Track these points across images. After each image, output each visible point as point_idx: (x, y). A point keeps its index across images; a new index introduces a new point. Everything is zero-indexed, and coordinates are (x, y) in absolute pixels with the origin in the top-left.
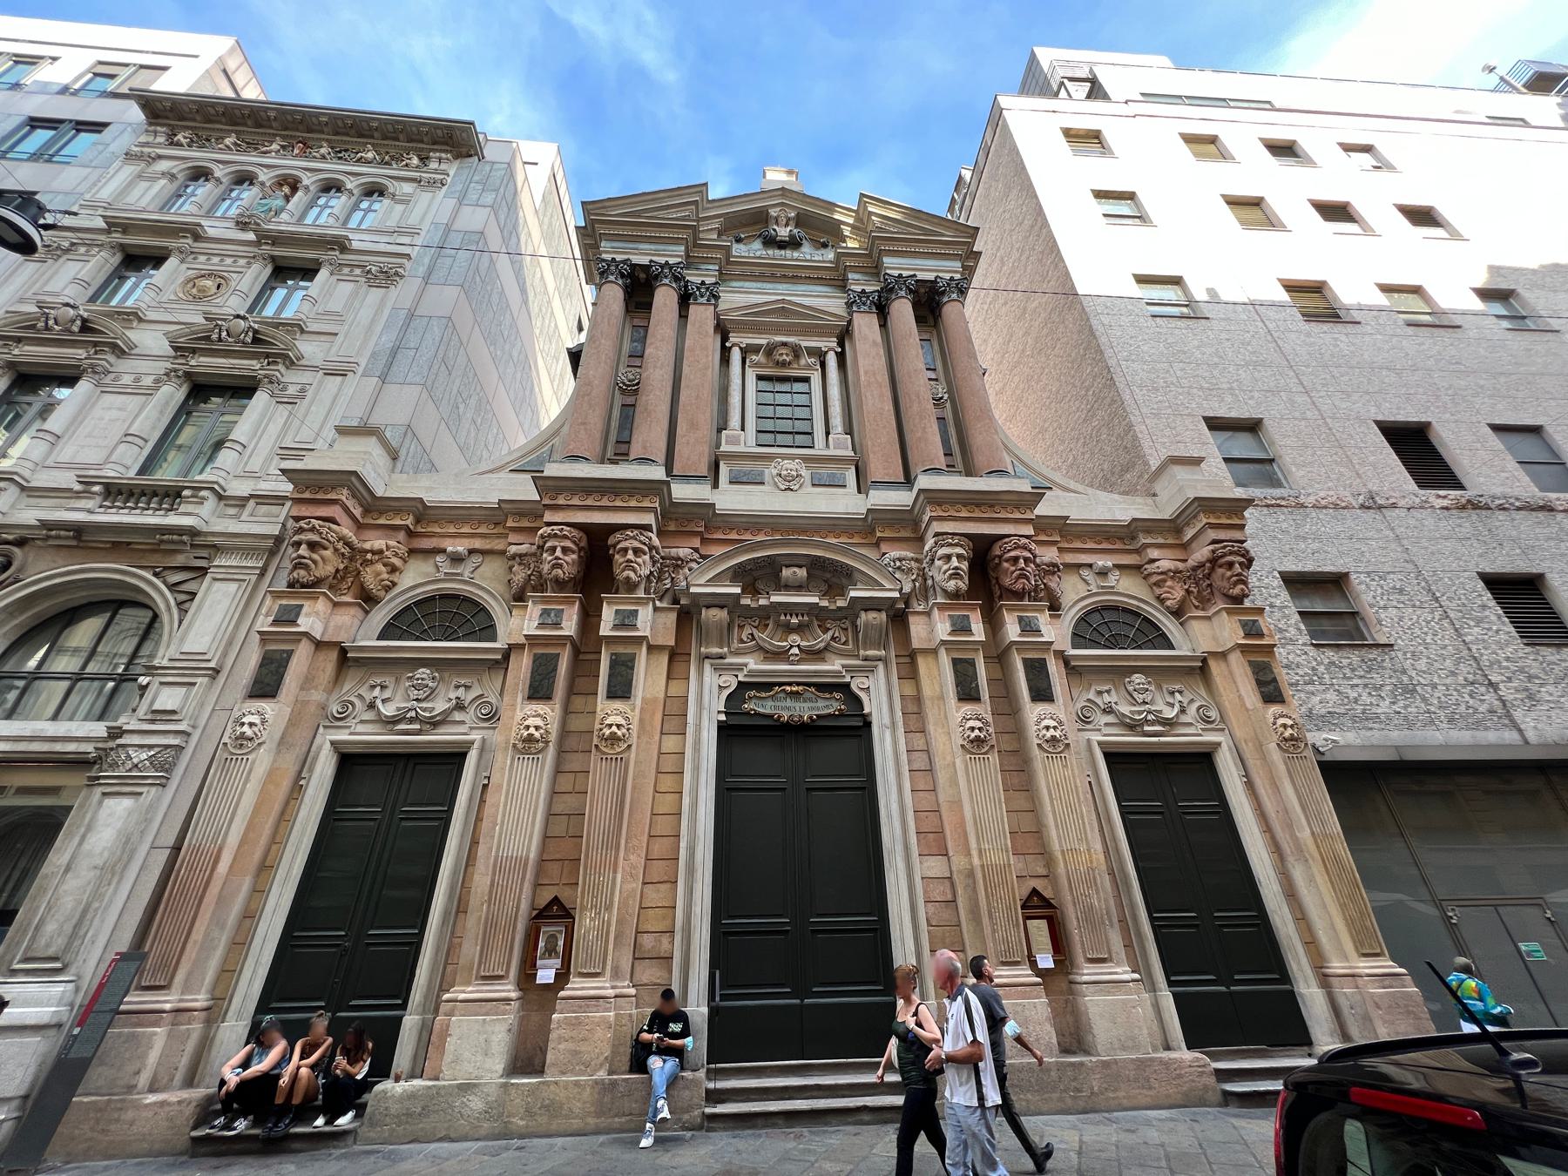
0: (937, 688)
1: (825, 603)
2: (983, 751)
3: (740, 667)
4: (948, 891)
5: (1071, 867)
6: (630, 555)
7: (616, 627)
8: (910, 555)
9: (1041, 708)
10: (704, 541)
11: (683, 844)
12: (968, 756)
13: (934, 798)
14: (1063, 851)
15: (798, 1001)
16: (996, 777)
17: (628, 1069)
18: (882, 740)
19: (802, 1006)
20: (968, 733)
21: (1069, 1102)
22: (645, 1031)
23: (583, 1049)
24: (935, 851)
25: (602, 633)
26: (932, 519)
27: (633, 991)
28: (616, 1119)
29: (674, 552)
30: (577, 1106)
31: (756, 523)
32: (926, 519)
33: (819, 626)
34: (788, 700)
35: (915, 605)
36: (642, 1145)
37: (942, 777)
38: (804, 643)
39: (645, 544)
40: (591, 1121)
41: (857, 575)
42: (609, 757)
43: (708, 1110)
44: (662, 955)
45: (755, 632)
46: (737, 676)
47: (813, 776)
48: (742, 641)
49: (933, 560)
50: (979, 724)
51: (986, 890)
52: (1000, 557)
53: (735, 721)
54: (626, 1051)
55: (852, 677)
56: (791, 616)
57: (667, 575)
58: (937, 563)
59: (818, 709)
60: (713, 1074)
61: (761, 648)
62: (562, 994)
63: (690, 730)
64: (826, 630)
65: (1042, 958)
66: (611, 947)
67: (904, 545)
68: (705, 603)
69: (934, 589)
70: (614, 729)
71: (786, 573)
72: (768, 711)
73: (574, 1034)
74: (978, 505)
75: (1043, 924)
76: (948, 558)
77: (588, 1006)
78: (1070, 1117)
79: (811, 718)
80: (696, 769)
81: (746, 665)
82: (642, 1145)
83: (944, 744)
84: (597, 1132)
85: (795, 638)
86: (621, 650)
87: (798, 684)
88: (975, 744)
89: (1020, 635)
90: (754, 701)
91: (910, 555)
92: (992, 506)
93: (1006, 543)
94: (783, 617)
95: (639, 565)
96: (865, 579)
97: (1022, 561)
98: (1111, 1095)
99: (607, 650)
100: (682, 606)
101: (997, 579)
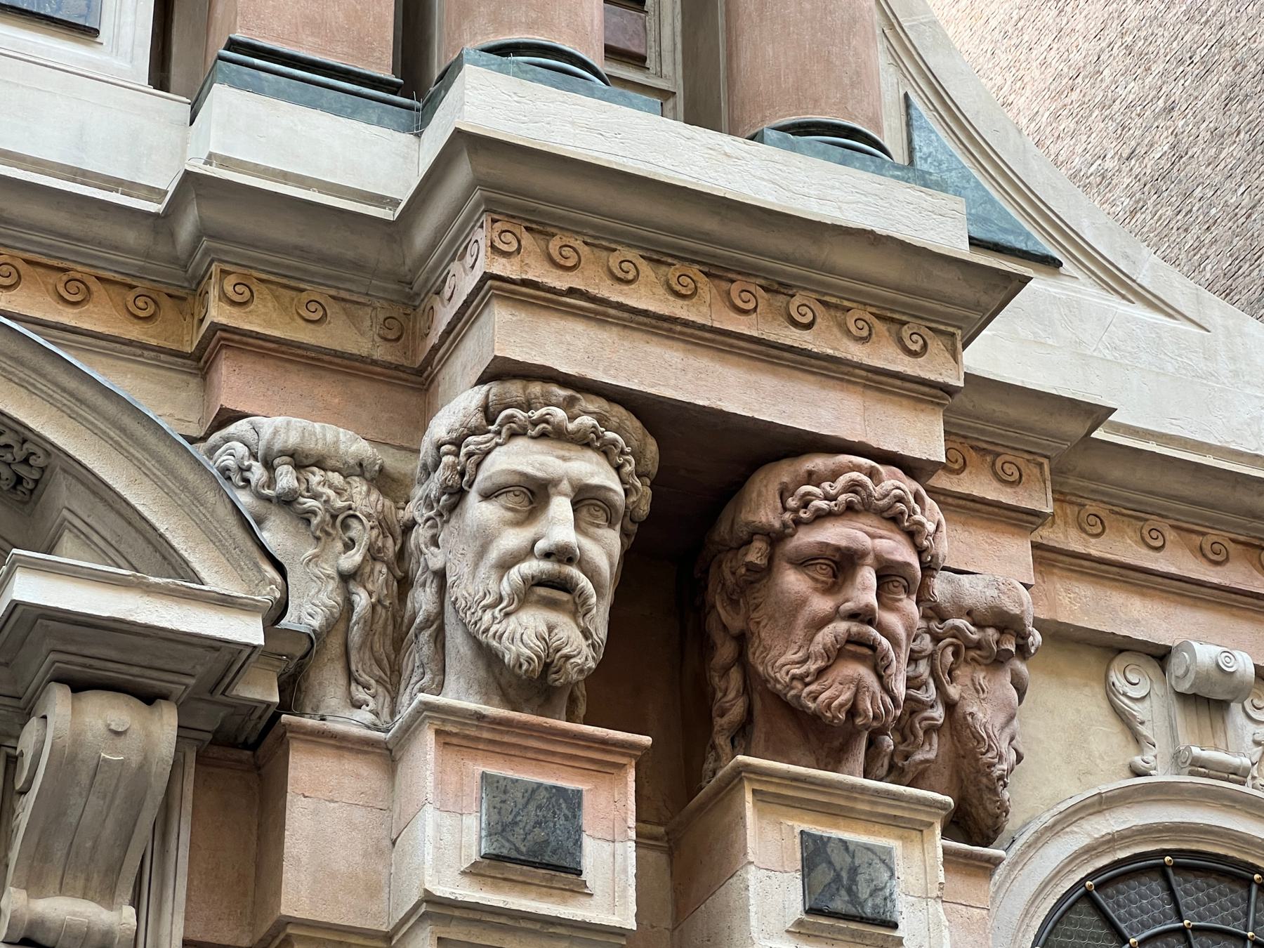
32: (463, 281)
49: (456, 495)
52: (775, 538)
58: (478, 511)
67: (327, 390)
74: (717, 271)
91: (354, 445)
93: (811, 478)
96: (107, 524)
101: (742, 640)
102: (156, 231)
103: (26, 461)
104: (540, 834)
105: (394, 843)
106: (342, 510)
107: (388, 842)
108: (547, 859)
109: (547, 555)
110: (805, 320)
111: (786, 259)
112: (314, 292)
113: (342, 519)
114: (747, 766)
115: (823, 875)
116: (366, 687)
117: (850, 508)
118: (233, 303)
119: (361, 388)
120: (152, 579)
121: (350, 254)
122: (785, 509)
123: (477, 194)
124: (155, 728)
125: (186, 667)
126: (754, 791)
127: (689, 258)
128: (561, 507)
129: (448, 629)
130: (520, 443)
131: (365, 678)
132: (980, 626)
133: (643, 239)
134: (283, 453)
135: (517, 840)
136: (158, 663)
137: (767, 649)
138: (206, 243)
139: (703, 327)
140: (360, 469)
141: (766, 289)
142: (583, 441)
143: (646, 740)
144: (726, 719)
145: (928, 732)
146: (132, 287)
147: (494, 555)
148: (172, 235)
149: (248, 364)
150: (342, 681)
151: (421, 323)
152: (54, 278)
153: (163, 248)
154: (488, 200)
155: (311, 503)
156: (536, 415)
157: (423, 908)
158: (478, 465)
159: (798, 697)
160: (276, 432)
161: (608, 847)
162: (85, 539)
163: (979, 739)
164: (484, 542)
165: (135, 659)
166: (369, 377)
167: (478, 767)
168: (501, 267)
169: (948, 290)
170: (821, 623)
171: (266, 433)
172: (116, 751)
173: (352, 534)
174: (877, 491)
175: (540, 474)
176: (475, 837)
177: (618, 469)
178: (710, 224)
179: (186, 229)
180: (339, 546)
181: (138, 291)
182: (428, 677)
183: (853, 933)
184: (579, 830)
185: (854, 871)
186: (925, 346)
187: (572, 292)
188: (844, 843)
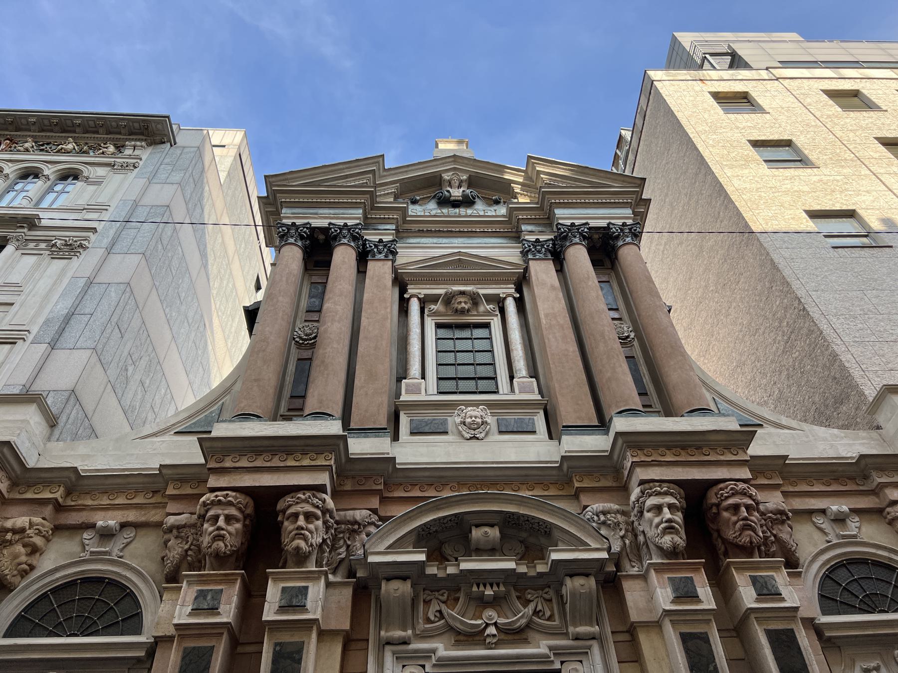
1: (523, 569)
8: (616, 507)
10: (384, 500)
26: (634, 465)
31: (442, 477)
33: (518, 598)
35: (628, 566)
38: (502, 621)
39: (317, 507)
41: (556, 534)
45: (444, 608)
46: (423, 666)
48: (428, 621)
52: (718, 505)
55: (562, 663)
56: (485, 586)
57: (342, 542)
58: (648, 515)
61: (450, 629)
64: (526, 603)
71: (477, 534)
74: (684, 448)
76: (658, 509)
81: (434, 651)
85: (491, 614)
92: (699, 448)
93: (721, 489)
94: (475, 589)
95: (311, 532)
97: (743, 509)
99: (270, 640)
101: (718, 531)
103: (546, 527)
104: (686, 589)
109: (666, 522)
112: (595, 475)
116: (634, 562)
126: (734, 568)
127: (676, 447)
131: (634, 560)
134: (600, 512)
138: (570, 470)
139: (684, 461)
140: (618, 512)
141: (696, 449)
142: (666, 494)
147: (654, 524)
148: (562, 470)
154: (626, 446)
155: (609, 522)
156: (653, 490)
157: (664, 613)
158: (644, 505)
164: (651, 522)
168: (635, 459)
171: (595, 509)
176: (671, 593)
177: (676, 498)
178: (679, 438)
180: (618, 530)
184: (695, 587)
185: (766, 583)
187: (652, 461)
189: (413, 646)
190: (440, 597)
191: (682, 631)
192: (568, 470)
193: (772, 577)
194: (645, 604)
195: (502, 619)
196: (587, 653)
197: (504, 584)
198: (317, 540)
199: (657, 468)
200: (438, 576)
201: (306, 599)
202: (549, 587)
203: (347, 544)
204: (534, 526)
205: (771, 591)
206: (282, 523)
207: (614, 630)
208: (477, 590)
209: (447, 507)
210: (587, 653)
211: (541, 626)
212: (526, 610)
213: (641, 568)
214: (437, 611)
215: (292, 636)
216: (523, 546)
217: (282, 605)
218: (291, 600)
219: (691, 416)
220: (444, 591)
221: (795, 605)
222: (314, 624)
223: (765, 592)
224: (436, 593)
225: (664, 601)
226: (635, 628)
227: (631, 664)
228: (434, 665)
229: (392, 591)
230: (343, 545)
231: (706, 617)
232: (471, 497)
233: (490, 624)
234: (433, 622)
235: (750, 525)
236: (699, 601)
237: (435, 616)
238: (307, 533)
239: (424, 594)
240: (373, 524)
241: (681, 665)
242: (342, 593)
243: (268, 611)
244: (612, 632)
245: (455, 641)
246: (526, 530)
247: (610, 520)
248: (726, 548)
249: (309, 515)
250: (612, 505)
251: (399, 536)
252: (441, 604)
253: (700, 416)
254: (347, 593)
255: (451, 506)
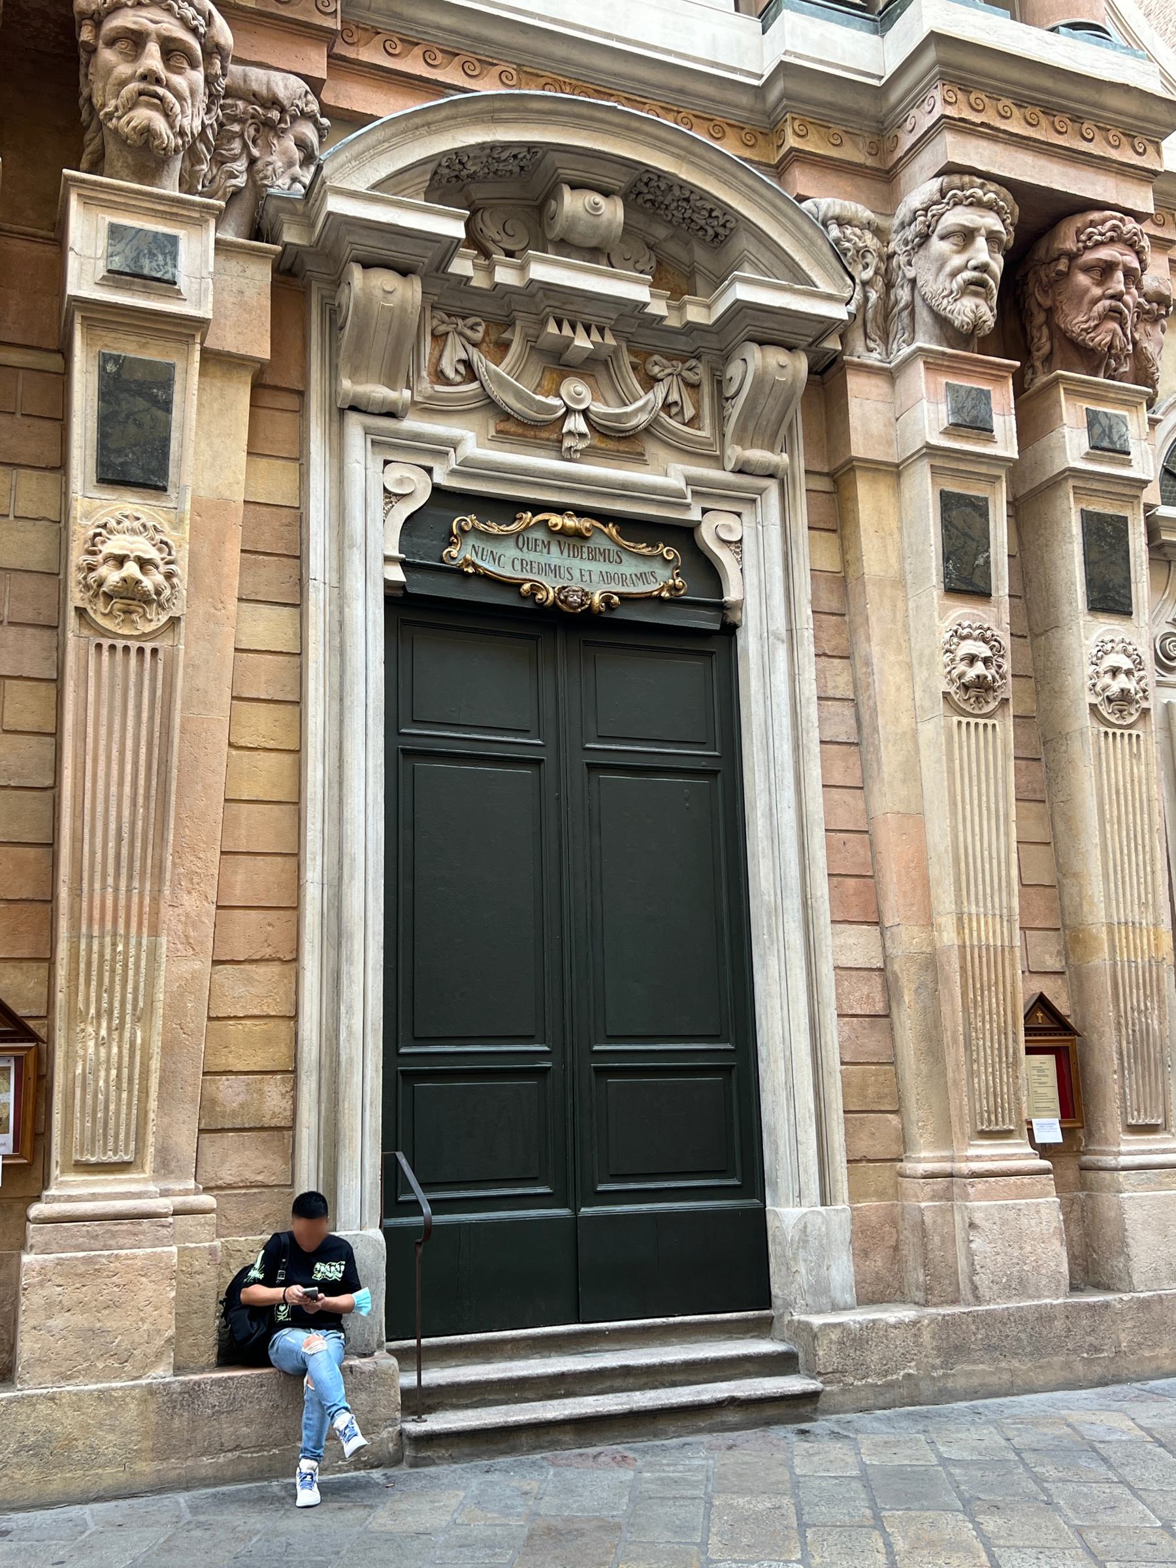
0: (893, 560)
1: (658, 308)
2: (987, 709)
3: (441, 448)
4: (878, 996)
5: (1122, 957)
6: (152, 59)
7: (115, 278)
8: (866, 214)
9: (1106, 627)
10: (336, 62)
11: (313, 874)
12: (956, 719)
13: (861, 805)
14: (1110, 926)
15: (564, 1212)
16: (1005, 768)
17: (213, 1359)
18: (767, 671)
19: (576, 1220)
20: (962, 667)
21: (1080, 1368)
22: (256, 1281)
23: (110, 1324)
24: (855, 915)
25: (72, 289)
26: (946, 123)
27: (208, 1200)
28: (205, 1460)
29: (258, 78)
30: (108, 1441)
31: (479, 40)
32: (923, 119)
33: (635, 368)
34: (554, 549)
35: (860, 347)
36: (300, 1503)
37: (889, 758)
38: (598, 408)
39: (194, 31)
40: (146, 1468)
41: (744, 243)
42: (120, 644)
43: (414, 1427)
44: (267, 1121)
45: (476, 356)
46: (429, 471)
47: (602, 738)
48: (440, 377)
49: (925, 237)
50: (983, 650)
51: (964, 994)
52: (1072, 257)
53: (427, 586)
54: (209, 1323)
55: (705, 511)
56: (573, 328)
57: (237, 145)
58: (937, 245)
59: (623, 579)
60: (416, 1359)
61: (490, 404)
62: (36, 1210)
63: (317, 598)
64: (650, 382)
65: (1042, 1125)
66: (153, 1104)
67: (845, 183)
68: (361, 252)
69: (912, 314)
70: (132, 569)
71: (573, 203)
72: (505, 571)
73: (86, 1294)
74: (1049, 110)
75: (1048, 1062)
76: (966, 236)
77: (114, 1235)
78: (1083, 1393)
79: (607, 600)
80: (339, 696)
81: (455, 444)
82: (300, 1503)
83: (898, 689)
84: (160, 1488)
85: (576, 390)
86: (129, 348)
87: (581, 512)
88: (972, 692)
89: (1088, 457)
90: (471, 541)
91: (866, 214)
92: (1077, 119)
93: (1092, 224)
94: (552, 328)
95: (179, 97)
96: (766, 258)
97: (1120, 275)
98: (1147, 1354)
99: (88, 343)
100: (286, 246)
101: (1050, 312)
102: (756, 96)
103: (724, 226)
104: (974, 412)
105: (897, 419)
106: (862, 248)
107: (893, 420)
108: (979, 425)
109: (975, 268)
110: (1090, 137)
111: (1082, 102)
112: (836, 129)
113: (862, 253)
114: (1062, 376)
115: (1097, 430)
116: (874, 341)
117: (1112, 240)
118: (799, 136)
119: (860, 181)
120: (797, 286)
121: (856, 106)
122: (1078, 241)
123: (937, 69)
124: (797, 363)
125: (808, 332)
126: (1065, 389)
127: (1035, 103)
128: (981, 242)
129: (917, 309)
130: (959, 209)
131: (873, 336)
132: (1149, 302)
133: (1015, 93)
134: (832, 218)
135: (964, 415)
136: (801, 332)
137: (1067, 316)
138: (785, 102)
139: (1043, 142)
140: (868, 226)
141: (1071, 120)
142: (990, 207)
143: (1018, 364)
144: (1041, 353)
145: (1125, 357)
146: (743, 129)
147: (948, 269)
148: (764, 99)
149: (808, 169)
150: (863, 338)
151: (888, 145)
152: (706, 124)
153: (759, 106)
154: (941, 73)
155: (847, 245)
156: (968, 193)
157: (924, 450)
158: (937, 221)
159: (1084, 340)
160: (829, 207)
161: (1001, 418)
162: (756, 267)
163: (1148, 360)
164: (942, 262)
165: (786, 328)
166: (864, 176)
167: (943, 380)
168: (950, 111)
169: (1159, 117)
170: (1096, 301)
171: (823, 207)
172: (782, 376)
173: (868, 260)
174: (1125, 229)
175: (971, 225)
176: (945, 415)
177: (1003, 221)
178: (1048, 83)
179: (774, 95)
180: (861, 267)
181: (746, 131)
182: (906, 335)
183: (1111, 458)
184: (991, 410)
185: (1111, 427)
186: (1145, 150)
187: (983, 124)
188: (1105, 413)
189: (411, 424)
190: (469, 332)
191: (947, 489)
192: (780, 100)
193: (1123, 420)
194: (882, 428)
195: (600, 405)
196: (754, 501)
197: (616, 333)
198: (193, 119)
199: (984, 144)
200: (473, 283)
201: (175, 266)
202: (698, 358)
203: (249, 154)
204: (695, 216)
205: (1115, 443)
206: (93, 51)
207: (811, 469)
208: (557, 332)
209: (515, 121)
210: (754, 501)
211: (674, 434)
212: (650, 395)
213: (884, 355)
214: (460, 361)
215: (144, 346)
216: (654, 258)
217: (115, 267)
218: (136, 259)
219: (1074, 37)
220: (479, 320)
221: (1144, 477)
222: (197, 329)
223: (1105, 443)
224: (460, 322)
225: (930, 426)
226: (853, 469)
227: (823, 534)
228: (453, 472)
229: (378, 293)
230: (241, 153)
231: (996, 472)
232: (577, 109)
233: (575, 411)
234: (448, 382)
235: (1121, 313)
236: (991, 440)
237: (457, 371)
238: (170, 97)
239: (433, 317)
240: (310, 117)
241: (933, 548)
242: (248, 273)
243: (80, 278)
244: (807, 472)
245: (498, 432)
246: (670, 222)
247: (849, 241)
248: (1051, 352)
249: (172, 46)
250: (860, 207)
251: (401, 165)
252: (470, 348)
253: (1088, 41)
254: (260, 276)
255: (527, 121)
